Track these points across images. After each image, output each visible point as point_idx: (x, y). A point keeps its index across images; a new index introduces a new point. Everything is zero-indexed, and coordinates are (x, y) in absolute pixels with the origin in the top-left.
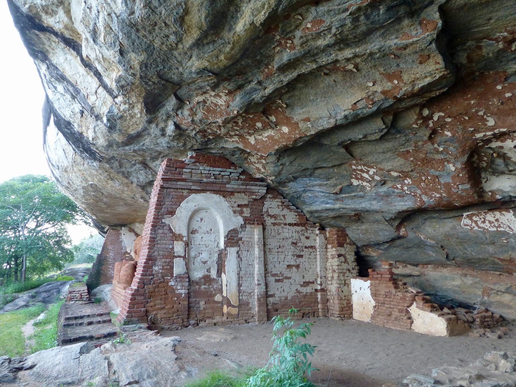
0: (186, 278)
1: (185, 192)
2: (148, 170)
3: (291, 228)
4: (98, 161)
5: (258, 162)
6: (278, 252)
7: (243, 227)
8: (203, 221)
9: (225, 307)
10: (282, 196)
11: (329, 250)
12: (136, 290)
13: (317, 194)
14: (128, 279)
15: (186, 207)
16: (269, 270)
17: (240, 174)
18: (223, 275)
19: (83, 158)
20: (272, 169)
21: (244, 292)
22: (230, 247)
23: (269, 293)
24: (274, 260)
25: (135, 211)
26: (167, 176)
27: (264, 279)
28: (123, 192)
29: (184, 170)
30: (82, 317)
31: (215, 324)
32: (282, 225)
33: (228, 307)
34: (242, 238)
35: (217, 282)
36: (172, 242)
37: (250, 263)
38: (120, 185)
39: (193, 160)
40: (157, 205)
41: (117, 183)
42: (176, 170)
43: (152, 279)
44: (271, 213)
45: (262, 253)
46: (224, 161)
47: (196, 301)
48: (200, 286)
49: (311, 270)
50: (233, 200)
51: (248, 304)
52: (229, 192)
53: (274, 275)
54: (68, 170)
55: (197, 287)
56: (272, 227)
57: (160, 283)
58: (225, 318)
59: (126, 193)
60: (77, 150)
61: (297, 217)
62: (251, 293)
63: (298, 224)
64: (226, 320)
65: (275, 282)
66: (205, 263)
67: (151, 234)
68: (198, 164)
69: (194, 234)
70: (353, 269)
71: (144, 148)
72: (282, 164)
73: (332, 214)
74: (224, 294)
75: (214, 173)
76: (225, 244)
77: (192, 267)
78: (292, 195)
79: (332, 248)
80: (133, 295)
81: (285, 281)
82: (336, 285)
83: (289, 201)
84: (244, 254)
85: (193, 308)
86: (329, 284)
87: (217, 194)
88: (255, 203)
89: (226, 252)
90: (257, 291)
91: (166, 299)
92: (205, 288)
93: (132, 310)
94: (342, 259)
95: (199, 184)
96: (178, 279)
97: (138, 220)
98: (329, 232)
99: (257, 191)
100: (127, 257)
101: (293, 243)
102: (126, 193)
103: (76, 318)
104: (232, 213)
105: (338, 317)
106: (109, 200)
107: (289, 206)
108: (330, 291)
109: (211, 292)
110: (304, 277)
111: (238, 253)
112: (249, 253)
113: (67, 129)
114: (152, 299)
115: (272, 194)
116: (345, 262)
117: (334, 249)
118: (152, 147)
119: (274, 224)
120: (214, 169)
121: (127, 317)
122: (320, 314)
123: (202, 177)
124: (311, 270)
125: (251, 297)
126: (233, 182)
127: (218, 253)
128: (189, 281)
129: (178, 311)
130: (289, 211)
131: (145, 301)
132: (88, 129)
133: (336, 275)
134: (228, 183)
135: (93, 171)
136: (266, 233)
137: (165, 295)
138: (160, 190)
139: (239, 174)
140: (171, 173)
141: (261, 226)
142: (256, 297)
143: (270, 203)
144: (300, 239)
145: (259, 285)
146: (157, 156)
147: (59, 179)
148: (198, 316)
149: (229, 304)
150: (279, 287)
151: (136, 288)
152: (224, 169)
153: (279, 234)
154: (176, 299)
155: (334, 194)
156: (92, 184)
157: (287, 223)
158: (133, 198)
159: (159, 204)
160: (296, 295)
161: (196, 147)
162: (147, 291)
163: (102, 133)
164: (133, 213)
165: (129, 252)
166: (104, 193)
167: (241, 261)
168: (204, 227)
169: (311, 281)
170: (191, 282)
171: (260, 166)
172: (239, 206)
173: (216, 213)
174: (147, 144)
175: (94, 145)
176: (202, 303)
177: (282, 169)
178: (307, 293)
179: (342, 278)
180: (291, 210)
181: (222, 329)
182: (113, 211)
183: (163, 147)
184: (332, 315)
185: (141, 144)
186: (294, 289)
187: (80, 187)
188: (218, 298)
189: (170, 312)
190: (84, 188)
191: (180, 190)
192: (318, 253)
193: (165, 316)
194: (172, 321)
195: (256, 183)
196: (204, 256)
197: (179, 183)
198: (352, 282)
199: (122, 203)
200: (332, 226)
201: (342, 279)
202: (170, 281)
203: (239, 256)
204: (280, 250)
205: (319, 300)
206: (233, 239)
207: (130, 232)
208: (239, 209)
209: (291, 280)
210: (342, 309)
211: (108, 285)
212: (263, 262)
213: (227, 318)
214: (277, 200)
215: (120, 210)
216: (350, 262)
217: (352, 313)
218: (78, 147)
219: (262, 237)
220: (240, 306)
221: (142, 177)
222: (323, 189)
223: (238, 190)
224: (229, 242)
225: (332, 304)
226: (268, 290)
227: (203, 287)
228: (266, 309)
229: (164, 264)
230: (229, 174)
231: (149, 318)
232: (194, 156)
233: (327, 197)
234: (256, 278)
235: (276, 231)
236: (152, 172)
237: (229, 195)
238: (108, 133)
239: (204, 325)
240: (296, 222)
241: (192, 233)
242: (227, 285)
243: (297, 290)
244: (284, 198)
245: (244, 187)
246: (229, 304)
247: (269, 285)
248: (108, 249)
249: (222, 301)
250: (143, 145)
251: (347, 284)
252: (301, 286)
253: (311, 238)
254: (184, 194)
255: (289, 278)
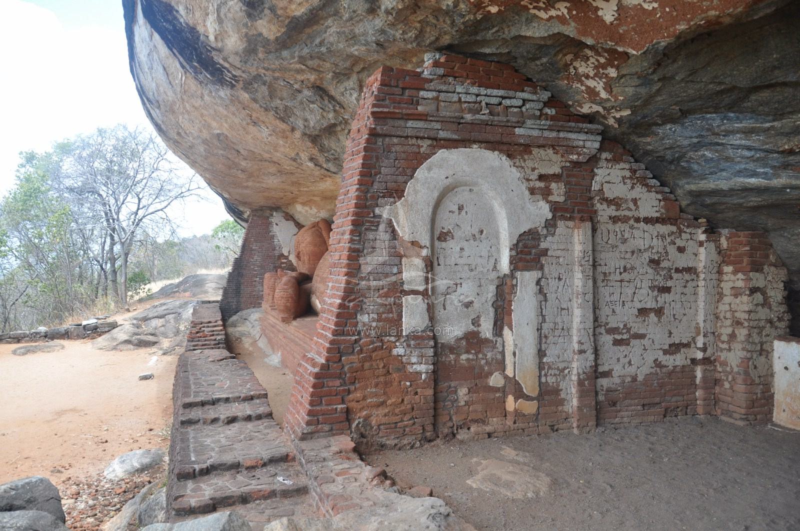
0: (429, 338)
1: (425, 144)
2: (326, 102)
3: (649, 227)
4: (227, 85)
5: (596, 75)
6: (621, 281)
7: (550, 225)
8: (463, 213)
9: (510, 399)
10: (632, 156)
11: (725, 277)
12: (323, 367)
13: (730, 152)
14: (288, 304)
15: (427, 179)
16: (603, 319)
17: (546, 104)
18: (506, 331)
19: (201, 83)
20: (630, 91)
21: (550, 368)
22: (522, 270)
23: (601, 369)
24: (612, 298)
25: (296, 184)
26: (383, 107)
27: (592, 339)
28: (276, 147)
29: (422, 93)
30: (214, 402)
31: (490, 435)
32: (632, 222)
33: (516, 399)
34: (547, 250)
35: (494, 347)
36: (396, 260)
37: (564, 306)
38: (270, 135)
39: (441, 71)
40: (362, 174)
41: (265, 132)
42: (403, 94)
43: (356, 341)
44: (609, 195)
45: (590, 283)
46: (509, 71)
47: (450, 387)
48: (459, 355)
49: (685, 319)
50: (530, 164)
51: (557, 391)
52: (521, 145)
53: (612, 331)
54: (176, 108)
55: (452, 357)
56: (610, 226)
57: (375, 350)
58: (509, 422)
59: (282, 149)
60: (188, 67)
61: (662, 203)
62: (565, 369)
63: (663, 219)
64: (512, 426)
65: (614, 344)
66: (468, 305)
67: (351, 241)
68: (451, 79)
69: (445, 240)
70: (780, 319)
71: (323, 49)
72: (663, 79)
73: (754, 200)
74: (509, 372)
75: (487, 100)
76: (511, 263)
77: (440, 313)
78: (661, 154)
79: (735, 273)
80: (317, 376)
81: (633, 342)
82: (743, 354)
83: (646, 169)
84: (552, 286)
85: (444, 401)
86: (722, 350)
87: (493, 150)
88: (576, 171)
89: (514, 282)
90: (577, 366)
91: (387, 384)
92: (468, 360)
93: (318, 408)
94: (759, 297)
95: (454, 126)
96: (412, 342)
97: (299, 200)
98: (728, 239)
99: (581, 143)
100: (284, 263)
101: (652, 261)
102: (282, 149)
103: (203, 404)
104: (527, 193)
105: (741, 419)
106: (250, 165)
107: (645, 178)
108: (724, 364)
109: (482, 368)
110: (670, 333)
111: (538, 283)
112: (562, 283)
113: (167, 21)
114: (357, 385)
115: (610, 151)
116: (763, 305)
117: (740, 276)
118: (341, 46)
119: (615, 220)
120: (489, 91)
121: (308, 423)
122: (700, 410)
123: (462, 111)
124: (685, 319)
125: (564, 377)
126: (529, 122)
127: (496, 282)
128: (435, 346)
129: (413, 409)
130: (645, 189)
131: (344, 390)
132: (207, 14)
133: (742, 333)
134: (521, 124)
135: (221, 109)
136: (598, 240)
137: (385, 375)
138: (368, 141)
139: (541, 105)
140: (394, 101)
141: (588, 225)
142: (574, 378)
143: (608, 171)
144: (667, 253)
145: (581, 352)
146: (354, 68)
147: (162, 126)
148: (454, 418)
149: (519, 394)
150: (621, 356)
151: (323, 361)
152: (511, 93)
153: (624, 241)
154: (408, 384)
155: (783, 152)
156: (218, 135)
157: (642, 216)
158: (294, 160)
159: (368, 173)
160: (653, 371)
161: (446, 40)
162: (346, 369)
163: (234, 20)
164: (292, 189)
165: (286, 254)
166: (242, 151)
167: (546, 300)
168: (467, 225)
169: (685, 341)
170: (439, 349)
171: (598, 85)
172: (541, 177)
173: (491, 194)
174: (331, 39)
175: (219, 50)
176: (463, 392)
177: (659, 91)
178: (675, 367)
179: (756, 339)
180: (649, 188)
181: (509, 452)
182: (258, 185)
183: (367, 43)
184: (729, 413)
185: (317, 41)
186: (650, 358)
187: (199, 141)
188: (495, 380)
189: (397, 411)
190: (205, 142)
191: (414, 141)
192: (701, 283)
193: (385, 420)
194: (401, 430)
195: (581, 125)
196: (467, 291)
197: (410, 124)
198: (775, 348)
199: (273, 169)
200: (738, 226)
201: (757, 341)
202: (396, 347)
203: (541, 291)
204: (626, 276)
205: (698, 381)
206: (528, 252)
207: (287, 220)
208: (542, 185)
209: (645, 342)
210: (752, 404)
211: (254, 310)
212: (591, 303)
213: (515, 423)
214: (622, 165)
215: (270, 181)
216: (774, 305)
217: (771, 412)
218: (189, 60)
219: (591, 248)
220: (540, 397)
221: (314, 116)
222: (755, 141)
223: (541, 142)
224: (521, 260)
225: (729, 392)
226: (599, 362)
227: (464, 357)
228: (594, 403)
229: (381, 310)
230: (520, 103)
231: (354, 426)
232: (442, 60)
233: (758, 160)
234: (575, 339)
235: (619, 236)
236: (334, 106)
237: (521, 154)
238: (246, 20)
239: (466, 437)
240: (658, 215)
241: (439, 239)
242: (514, 354)
243: (656, 360)
244: (636, 161)
245: (554, 134)
246: (519, 394)
247: (600, 352)
248: (252, 250)
249: (505, 387)
250: (321, 44)
251: (765, 352)
252: (665, 352)
253: (689, 250)
254: (422, 150)
255: (642, 336)
